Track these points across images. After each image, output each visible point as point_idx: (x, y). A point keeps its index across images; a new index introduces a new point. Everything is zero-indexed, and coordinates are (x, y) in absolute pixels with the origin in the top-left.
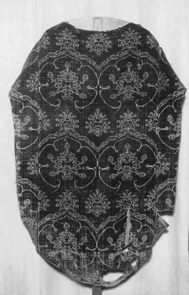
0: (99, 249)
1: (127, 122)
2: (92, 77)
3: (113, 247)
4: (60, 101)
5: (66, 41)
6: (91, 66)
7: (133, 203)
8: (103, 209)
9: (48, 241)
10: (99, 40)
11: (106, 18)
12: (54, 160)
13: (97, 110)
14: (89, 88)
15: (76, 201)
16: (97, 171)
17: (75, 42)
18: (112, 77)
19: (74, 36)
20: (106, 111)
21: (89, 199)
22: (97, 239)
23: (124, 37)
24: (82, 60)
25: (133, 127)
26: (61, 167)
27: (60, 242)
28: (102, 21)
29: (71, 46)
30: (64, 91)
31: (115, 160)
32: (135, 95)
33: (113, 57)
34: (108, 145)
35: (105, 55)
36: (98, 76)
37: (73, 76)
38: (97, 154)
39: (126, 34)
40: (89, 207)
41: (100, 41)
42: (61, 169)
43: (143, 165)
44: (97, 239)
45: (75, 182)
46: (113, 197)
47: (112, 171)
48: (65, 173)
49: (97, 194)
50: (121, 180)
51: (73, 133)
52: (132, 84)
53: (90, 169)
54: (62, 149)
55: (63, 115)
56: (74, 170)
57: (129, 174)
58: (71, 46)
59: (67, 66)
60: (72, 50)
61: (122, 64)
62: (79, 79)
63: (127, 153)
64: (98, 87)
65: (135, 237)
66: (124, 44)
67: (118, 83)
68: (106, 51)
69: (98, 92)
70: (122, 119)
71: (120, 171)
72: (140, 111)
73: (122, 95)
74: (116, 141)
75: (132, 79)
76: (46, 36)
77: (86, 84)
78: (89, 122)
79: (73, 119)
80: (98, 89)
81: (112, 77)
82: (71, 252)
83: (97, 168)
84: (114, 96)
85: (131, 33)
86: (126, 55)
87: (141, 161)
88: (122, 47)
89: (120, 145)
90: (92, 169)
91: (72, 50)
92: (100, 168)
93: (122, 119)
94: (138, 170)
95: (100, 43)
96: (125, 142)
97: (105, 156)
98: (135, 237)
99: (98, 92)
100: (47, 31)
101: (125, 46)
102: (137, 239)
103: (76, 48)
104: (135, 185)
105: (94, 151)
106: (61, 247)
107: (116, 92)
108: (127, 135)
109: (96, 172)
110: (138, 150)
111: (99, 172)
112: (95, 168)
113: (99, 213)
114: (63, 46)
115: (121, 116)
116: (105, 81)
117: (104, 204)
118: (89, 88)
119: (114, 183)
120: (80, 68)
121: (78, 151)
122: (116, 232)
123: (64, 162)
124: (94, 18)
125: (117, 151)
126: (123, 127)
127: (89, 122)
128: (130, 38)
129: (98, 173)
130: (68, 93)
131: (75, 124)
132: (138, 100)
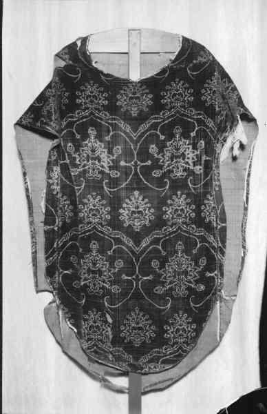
0: (138, 163)
2: (129, 263)
4: (80, 71)
7: (186, 96)
8: (142, 104)
10: (134, 93)
11: (148, 30)
13: (135, 193)
14: (124, 277)
15: (104, 95)
16: (137, 279)
18: (153, 149)
19: (102, 89)
21: (122, 92)
23: (171, 205)
25: (186, 217)
28: (140, 33)
33: (156, 234)
34: (151, 243)
37: (103, 264)
41: (139, 210)
43: (202, 274)
47: (157, 281)
49: (137, 197)
50: (172, 297)
51: (103, 226)
52: (186, 273)
53: (126, 278)
55: (86, 87)
57: (183, 287)
63: (180, 255)
64: (136, 163)
66: (169, 100)
68: (144, 109)
70: (171, 205)
71: (171, 283)
72: (197, 311)
73: (171, 171)
77: (120, 272)
81: (153, 149)
82: (99, 169)
83: (137, 276)
86: (172, 116)
89: (169, 243)
90: (130, 278)
91: (98, 109)
92: (140, 277)
95: (139, 212)
97: (147, 262)
98: (191, 260)
99: (137, 285)
103: (103, 106)
105: (133, 252)
106: (85, 162)
108: (177, 230)
109: (133, 168)
110: (194, 252)
112: (134, 277)
116: (144, 154)
117: (147, 328)
118: (124, 277)
119: (160, 182)
120: (112, 251)
122: (162, 137)
124: (129, 30)
125: (164, 253)
130: (95, 285)
131: (105, 213)
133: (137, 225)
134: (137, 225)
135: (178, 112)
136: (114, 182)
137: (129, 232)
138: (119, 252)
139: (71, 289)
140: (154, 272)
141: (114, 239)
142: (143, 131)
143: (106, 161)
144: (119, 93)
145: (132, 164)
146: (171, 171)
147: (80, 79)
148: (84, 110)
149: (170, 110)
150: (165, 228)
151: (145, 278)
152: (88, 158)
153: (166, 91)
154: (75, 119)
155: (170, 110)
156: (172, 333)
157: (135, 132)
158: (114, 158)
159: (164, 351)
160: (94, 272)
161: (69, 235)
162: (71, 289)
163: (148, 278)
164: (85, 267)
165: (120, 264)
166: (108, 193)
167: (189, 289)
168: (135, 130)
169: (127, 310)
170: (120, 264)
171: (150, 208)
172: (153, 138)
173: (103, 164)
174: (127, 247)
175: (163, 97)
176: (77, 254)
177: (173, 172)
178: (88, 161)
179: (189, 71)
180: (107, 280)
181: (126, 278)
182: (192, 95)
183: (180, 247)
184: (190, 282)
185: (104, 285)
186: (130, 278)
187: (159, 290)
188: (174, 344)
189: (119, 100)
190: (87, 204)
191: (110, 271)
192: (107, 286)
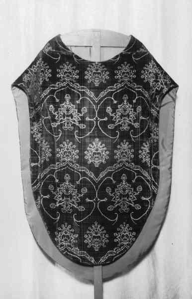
1: (123, 236)
3: (112, 117)
5: (67, 73)
6: (90, 97)
9: (51, 113)
12: (54, 191)
17: (75, 74)
20: (103, 223)
22: (97, 188)
23: (119, 149)
24: (81, 172)
26: (61, 199)
27: (61, 193)
29: (71, 78)
30: (64, 204)
31: (113, 191)
32: (130, 125)
33: (109, 169)
35: (102, 167)
36: (97, 190)
38: (97, 185)
39: (122, 67)
40: (88, 156)
42: (61, 121)
44: (97, 109)
45: (74, 215)
46: (111, 230)
48: (65, 206)
52: (128, 196)
53: (89, 201)
54: (62, 180)
56: (73, 203)
57: (126, 206)
58: (71, 78)
59: (67, 98)
60: (70, 246)
61: (117, 176)
62: (78, 112)
64: (97, 199)
65: (132, 108)
67: (114, 195)
69: (96, 205)
74: (115, 91)
75: (127, 112)
76: (49, 46)
78: (88, 72)
79: (73, 69)
80: (96, 202)
81: (109, 109)
84: (110, 208)
85: (126, 145)
86: (122, 87)
87: (137, 192)
88: (118, 79)
91: (72, 162)
93: (119, 231)
94: (134, 201)
95: (98, 153)
96: (120, 173)
97: (103, 188)
100: (49, 42)
101: (122, 78)
102: (132, 109)
103: (76, 79)
104: (133, 57)
107: (113, 203)
109: (95, 122)
111: (99, 122)
113: (99, 162)
114: (63, 77)
115: (118, 147)
116: (102, 113)
121: (78, 183)
123: (64, 113)
126: (121, 241)
127: (88, 72)
128: (124, 150)
129: (96, 205)
132: (132, 131)
137: (91, 167)
138: (84, 182)
142: (102, 97)
150: (115, 164)
151: (102, 201)
154: (56, 89)
155: (121, 83)
156: (119, 238)
160: (67, 196)
165: (85, 190)
166: (78, 140)
169: (89, 224)
174: (90, 178)
177: (121, 126)
181: (89, 201)
182: (135, 74)
183: (124, 177)
192: (75, 206)
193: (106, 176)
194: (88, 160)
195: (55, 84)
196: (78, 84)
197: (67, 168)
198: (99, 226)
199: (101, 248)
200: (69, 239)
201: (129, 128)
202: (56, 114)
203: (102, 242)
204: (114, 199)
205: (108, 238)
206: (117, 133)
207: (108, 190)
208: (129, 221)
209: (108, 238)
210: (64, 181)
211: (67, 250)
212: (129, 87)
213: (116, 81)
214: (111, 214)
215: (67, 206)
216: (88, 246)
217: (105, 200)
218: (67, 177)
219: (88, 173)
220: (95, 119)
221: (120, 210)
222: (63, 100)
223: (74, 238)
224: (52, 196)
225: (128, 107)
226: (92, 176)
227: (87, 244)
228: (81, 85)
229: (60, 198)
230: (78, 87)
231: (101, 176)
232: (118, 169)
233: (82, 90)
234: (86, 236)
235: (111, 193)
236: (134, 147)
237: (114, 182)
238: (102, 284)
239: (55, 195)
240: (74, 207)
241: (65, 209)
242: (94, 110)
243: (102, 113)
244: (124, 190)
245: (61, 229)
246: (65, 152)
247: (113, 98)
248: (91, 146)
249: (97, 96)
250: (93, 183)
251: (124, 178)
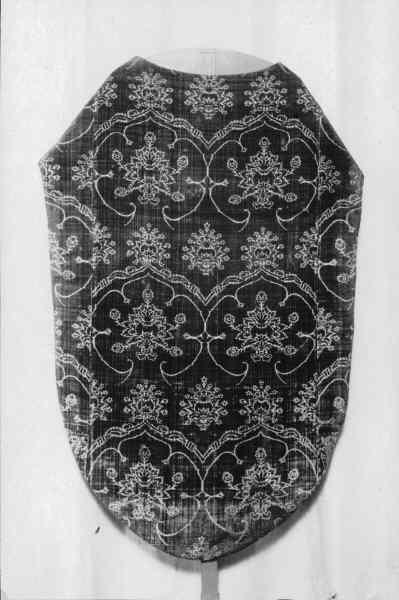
1: (258, 404)
3: (239, 179)
21: (187, 396)
22: (202, 473)
33: (235, 125)
35: (221, 120)
38: (205, 310)
41: (212, 93)
43: (292, 333)
46: (234, 394)
52: (271, 177)
53: (190, 337)
56: (160, 341)
57: (266, 349)
59: (150, 138)
69: (205, 345)
80: (205, 340)
83: (205, 335)
84: (234, 200)
88: (251, 108)
90: (195, 338)
91: (154, 422)
93: (255, 88)
103: (166, 105)
108: (259, 275)
125: (241, 305)
129: (205, 345)
133: (207, 268)
134: (207, 268)
135: (262, 273)
136: (172, 364)
137: (195, 276)
138: (179, 306)
139: (110, 197)
140: (230, 176)
141: (172, 443)
142: (218, 139)
143: (166, 179)
144: (182, 398)
145: (204, 186)
146: (252, 199)
147: (130, 377)
148: (140, 110)
149: (252, 271)
150: (246, 117)
152: (140, 329)
153: (246, 398)
154: (126, 121)
155: (252, 271)
156: (251, 254)
157: (205, 296)
158: (173, 488)
159: (245, 123)
160: (150, 173)
161: (110, 123)
162: (109, 355)
163: (219, 337)
164: (137, 167)
165: (181, 319)
166: (163, 541)
167: (273, 350)
168: (205, 293)
169: (191, 380)
170: (181, 319)
171: (223, 246)
172: (226, 463)
173: (158, 497)
174: (195, 139)
175: (242, 407)
176: (122, 146)
177: (255, 200)
178: (137, 492)
179: (279, 218)
180: (163, 340)
181: (190, 337)
182: (280, 405)
183: (261, 298)
184: (274, 342)
185: (163, 191)
186: (195, 338)
187: (118, 348)
188: (254, 268)
189: (182, 408)
190: (138, 239)
191: (168, 327)
192: (166, 193)
193: (224, 293)
194: (188, 262)
195: (123, 269)
196: (171, 115)
197: (150, 121)
198: (209, 388)
199: (213, 427)
200: (157, 96)
201: (271, 204)
202: (120, 484)
203: (214, 415)
204: (241, 336)
205: (226, 408)
206: (245, 365)
207: (232, 163)
208: (271, 380)
209: (226, 408)
210: (141, 301)
211: (153, 116)
212: (268, 278)
213: (243, 266)
214: (237, 363)
215: (147, 347)
216: (189, 266)
217: (225, 183)
218: (148, 295)
219: (191, 130)
220: (204, 181)
221: (254, 204)
222: (139, 143)
223: (161, 406)
224: (120, 173)
225: (272, 161)
226: (197, 292)
227: (188, 262)
228: (173, 272)
229: (135, 176)
230: (167, 433)
231: (217, 136)
232: (253, 126)
233: (177, 282)
234: (182, 404)
235: (235, 325)
236: (284, 241)
237: (244, 150)
238: (217, 575)
239: (124, 172)
240: (164, 194)
241: (146, 198)
242: (203, 162)
243: (219, 170)
244: (264, 167)
245: (139, 235)
246: (144, 247)
247: (239, 143)
248: (196, 236)
249: (206, 294)
250: (200, 307)
251: (265, 144)
